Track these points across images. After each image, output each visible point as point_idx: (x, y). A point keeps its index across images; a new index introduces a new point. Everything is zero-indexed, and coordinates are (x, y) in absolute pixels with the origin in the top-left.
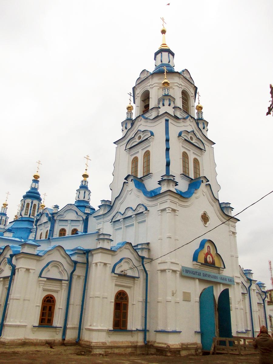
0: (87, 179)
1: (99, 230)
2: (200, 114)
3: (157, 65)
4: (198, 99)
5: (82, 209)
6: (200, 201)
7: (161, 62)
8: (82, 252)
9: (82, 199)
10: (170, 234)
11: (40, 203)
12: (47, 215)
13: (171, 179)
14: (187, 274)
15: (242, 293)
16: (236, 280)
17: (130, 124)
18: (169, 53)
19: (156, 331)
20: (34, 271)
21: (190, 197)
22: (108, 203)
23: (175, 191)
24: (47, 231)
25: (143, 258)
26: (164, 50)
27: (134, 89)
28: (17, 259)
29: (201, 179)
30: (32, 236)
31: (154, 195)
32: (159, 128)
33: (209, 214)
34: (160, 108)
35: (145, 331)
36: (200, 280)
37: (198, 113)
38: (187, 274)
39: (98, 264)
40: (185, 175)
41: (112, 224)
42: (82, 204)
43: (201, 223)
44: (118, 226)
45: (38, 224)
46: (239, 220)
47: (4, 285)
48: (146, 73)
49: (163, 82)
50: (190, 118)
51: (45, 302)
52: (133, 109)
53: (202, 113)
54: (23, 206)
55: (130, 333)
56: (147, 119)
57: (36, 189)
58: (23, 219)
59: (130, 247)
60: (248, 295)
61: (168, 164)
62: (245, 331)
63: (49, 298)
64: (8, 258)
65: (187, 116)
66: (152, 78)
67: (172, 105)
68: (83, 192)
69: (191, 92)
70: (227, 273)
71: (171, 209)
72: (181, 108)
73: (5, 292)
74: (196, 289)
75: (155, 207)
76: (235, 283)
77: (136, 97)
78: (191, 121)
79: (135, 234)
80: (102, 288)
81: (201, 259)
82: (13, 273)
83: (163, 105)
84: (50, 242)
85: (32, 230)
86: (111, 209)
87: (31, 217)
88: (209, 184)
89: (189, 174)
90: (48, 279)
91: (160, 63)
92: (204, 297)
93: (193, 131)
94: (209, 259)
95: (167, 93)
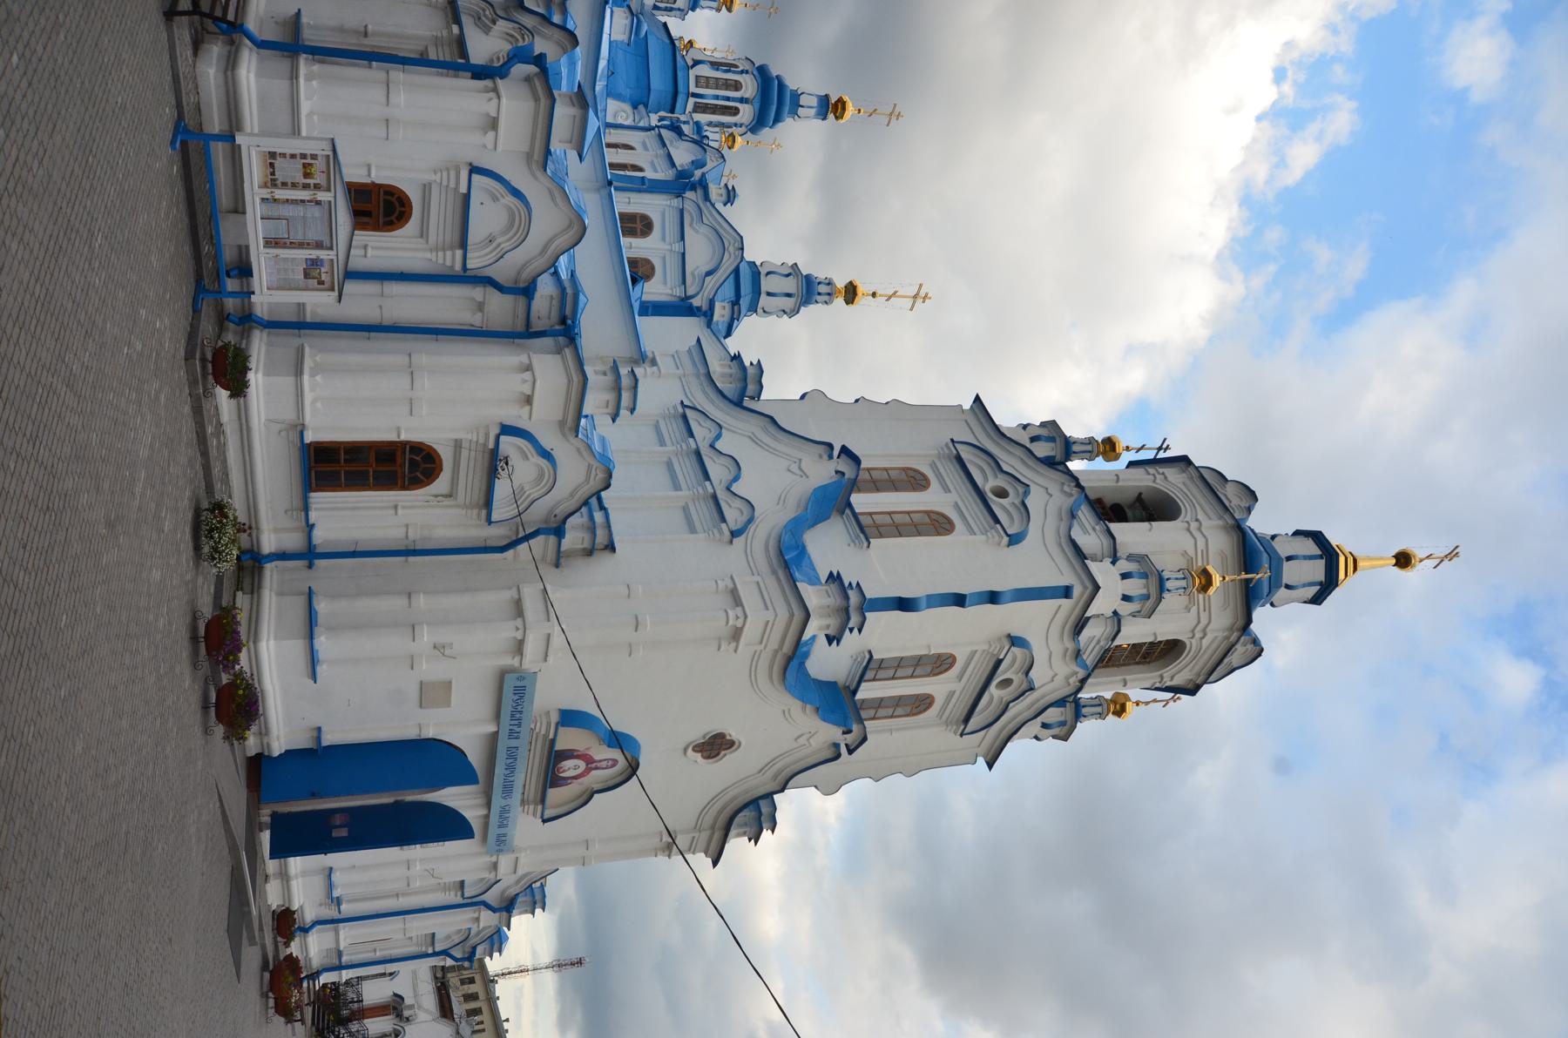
0: (839, 301)
1: (654, 362)
2: (1099, 709)
3: (1276, 544)
4: (1155, 701)
5: (728, 291)
6: (774, 725)
7: (1289, 558)
8: (568, 311)
9: (764, 288)
10: (652, 631)
11: (743, 129)
12: (699, 164)
13: (849, 619)
14: (511, 691)
15: (462, 883)
16: (505, 862)
17: (1052, 454)
18: (1320, 583)
19: (310, 593)
20: (490, 146)
21: (788, 689)
22: (751, 388)
23: (806, 636)
24: (641, 170)
25: (559, 532)
26: (1331, 566)
27: (1184, 461)
28: (528, 79)
29: (855, 727)
30: (617, 110)
31: (789, 559)
32: (1037, 562)
33: (729, 760)
34: (1113, 563)
35: (309, 554)
36: (494, 738)
37: (1099, 702)
38: (511, 691)
39: (527, 375)
40: (870, 667)
41: (675, 407)
42: (747, 288)
43: (698, 733)
44: (672, 429)
45: (664, 132)
46: (715, 863)
47: (437, 41)
48: (1244, 504)
49: (1210, 569)
50: (1082, 674)
51: (386, 193)
52: (1108, 460)
53: (1101, 716)
54: (730, 67)
55: (297, 502)
56: (1073, 516)
57: (794, 113)
58: (680, 74)
59: (594, 484)
60: (459, 900)
61: (904, 604)
62: (336, 894)
63: (399, 209)
64: (531, 45)
65: (1088, 662)
66: (1225, 528)
67: (1125, 609)
68: (792, 290)
69: (1180, 672)
70: (526, 827)
71: (739, 624)
72: (1116, 643)
73: (408, 49)
74: (464, 725)
75: (744, 563)
76: (494, 859)
77: (1151, 471)
78: (1067, 679)
79: (643, 497)
80: (445, 398)
81: (569, 739)
82: (480, 73)
83: (1125, 576)
84: (598, 190)
85: (641, 107)
86: (730, 401)
87: (692, 101)
88: (838, 756)
89: (874, 680)
90: (467, 198)
91: (1283, 554)
92: (441, 760)
93: (1032, 689)
94: (570, 767)
95: (1168, 585)
